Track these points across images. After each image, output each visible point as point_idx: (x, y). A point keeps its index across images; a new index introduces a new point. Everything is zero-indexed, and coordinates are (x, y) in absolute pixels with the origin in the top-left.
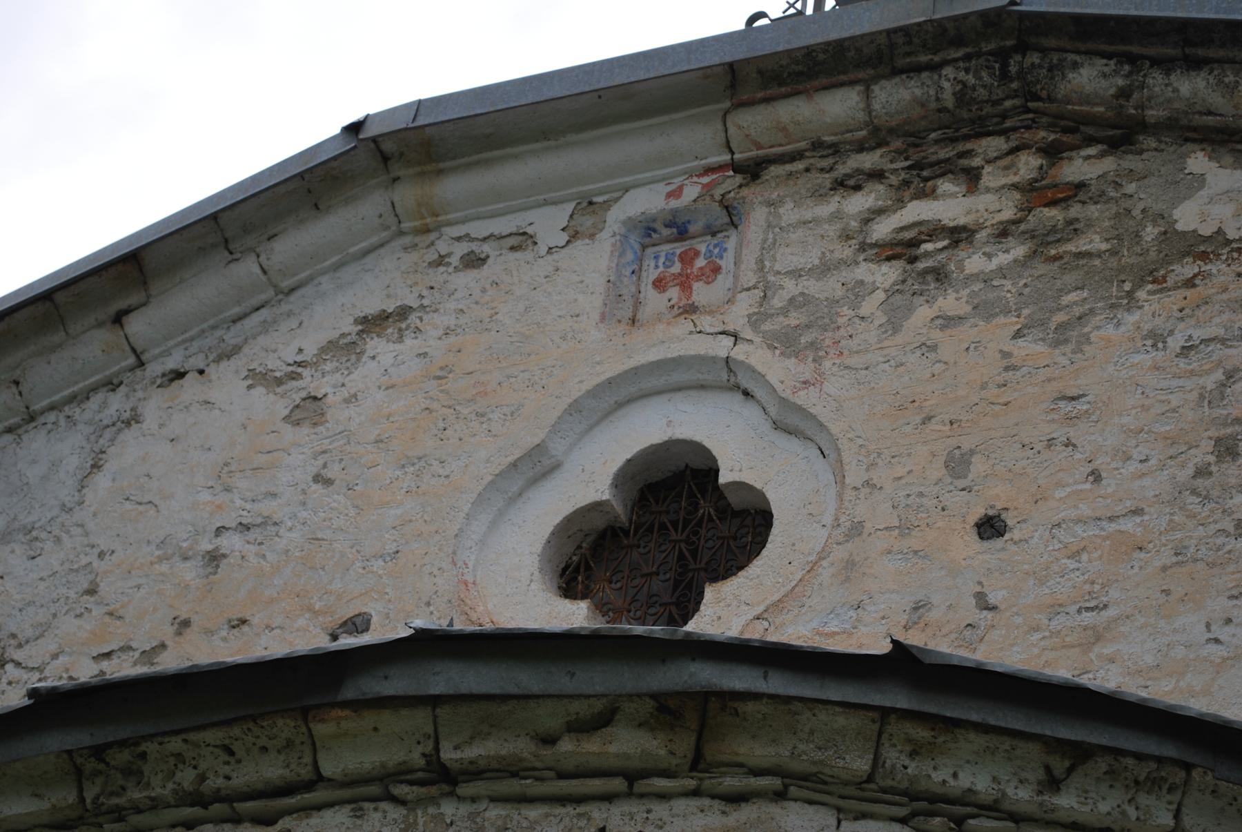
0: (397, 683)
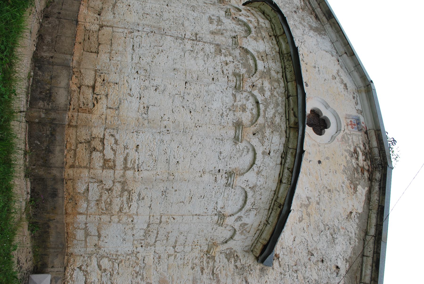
0: (299, 91)
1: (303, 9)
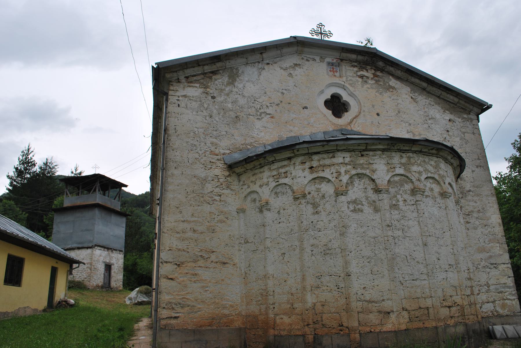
1: (206, 87)
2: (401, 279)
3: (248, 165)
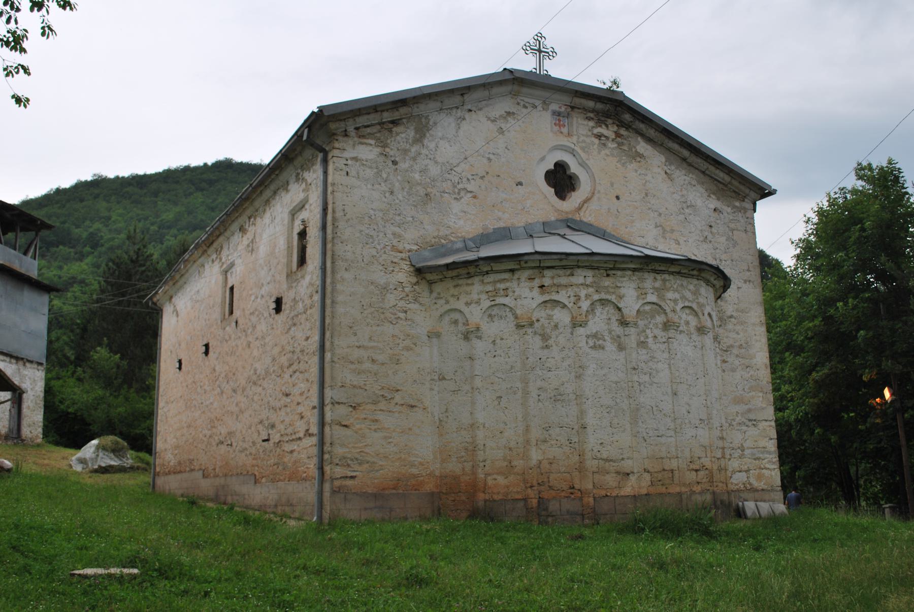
1: (385, 146)
2: (645, 434)
3: (450, 272)
